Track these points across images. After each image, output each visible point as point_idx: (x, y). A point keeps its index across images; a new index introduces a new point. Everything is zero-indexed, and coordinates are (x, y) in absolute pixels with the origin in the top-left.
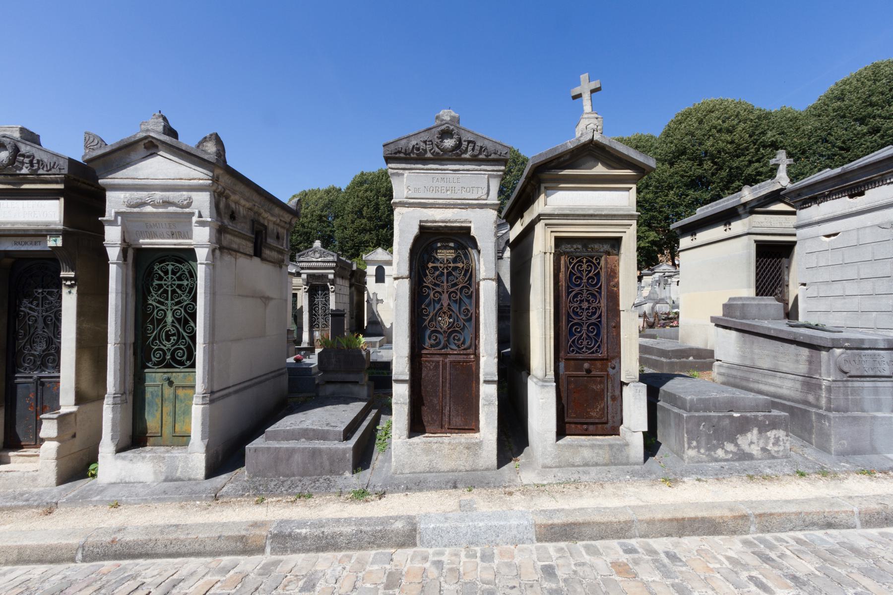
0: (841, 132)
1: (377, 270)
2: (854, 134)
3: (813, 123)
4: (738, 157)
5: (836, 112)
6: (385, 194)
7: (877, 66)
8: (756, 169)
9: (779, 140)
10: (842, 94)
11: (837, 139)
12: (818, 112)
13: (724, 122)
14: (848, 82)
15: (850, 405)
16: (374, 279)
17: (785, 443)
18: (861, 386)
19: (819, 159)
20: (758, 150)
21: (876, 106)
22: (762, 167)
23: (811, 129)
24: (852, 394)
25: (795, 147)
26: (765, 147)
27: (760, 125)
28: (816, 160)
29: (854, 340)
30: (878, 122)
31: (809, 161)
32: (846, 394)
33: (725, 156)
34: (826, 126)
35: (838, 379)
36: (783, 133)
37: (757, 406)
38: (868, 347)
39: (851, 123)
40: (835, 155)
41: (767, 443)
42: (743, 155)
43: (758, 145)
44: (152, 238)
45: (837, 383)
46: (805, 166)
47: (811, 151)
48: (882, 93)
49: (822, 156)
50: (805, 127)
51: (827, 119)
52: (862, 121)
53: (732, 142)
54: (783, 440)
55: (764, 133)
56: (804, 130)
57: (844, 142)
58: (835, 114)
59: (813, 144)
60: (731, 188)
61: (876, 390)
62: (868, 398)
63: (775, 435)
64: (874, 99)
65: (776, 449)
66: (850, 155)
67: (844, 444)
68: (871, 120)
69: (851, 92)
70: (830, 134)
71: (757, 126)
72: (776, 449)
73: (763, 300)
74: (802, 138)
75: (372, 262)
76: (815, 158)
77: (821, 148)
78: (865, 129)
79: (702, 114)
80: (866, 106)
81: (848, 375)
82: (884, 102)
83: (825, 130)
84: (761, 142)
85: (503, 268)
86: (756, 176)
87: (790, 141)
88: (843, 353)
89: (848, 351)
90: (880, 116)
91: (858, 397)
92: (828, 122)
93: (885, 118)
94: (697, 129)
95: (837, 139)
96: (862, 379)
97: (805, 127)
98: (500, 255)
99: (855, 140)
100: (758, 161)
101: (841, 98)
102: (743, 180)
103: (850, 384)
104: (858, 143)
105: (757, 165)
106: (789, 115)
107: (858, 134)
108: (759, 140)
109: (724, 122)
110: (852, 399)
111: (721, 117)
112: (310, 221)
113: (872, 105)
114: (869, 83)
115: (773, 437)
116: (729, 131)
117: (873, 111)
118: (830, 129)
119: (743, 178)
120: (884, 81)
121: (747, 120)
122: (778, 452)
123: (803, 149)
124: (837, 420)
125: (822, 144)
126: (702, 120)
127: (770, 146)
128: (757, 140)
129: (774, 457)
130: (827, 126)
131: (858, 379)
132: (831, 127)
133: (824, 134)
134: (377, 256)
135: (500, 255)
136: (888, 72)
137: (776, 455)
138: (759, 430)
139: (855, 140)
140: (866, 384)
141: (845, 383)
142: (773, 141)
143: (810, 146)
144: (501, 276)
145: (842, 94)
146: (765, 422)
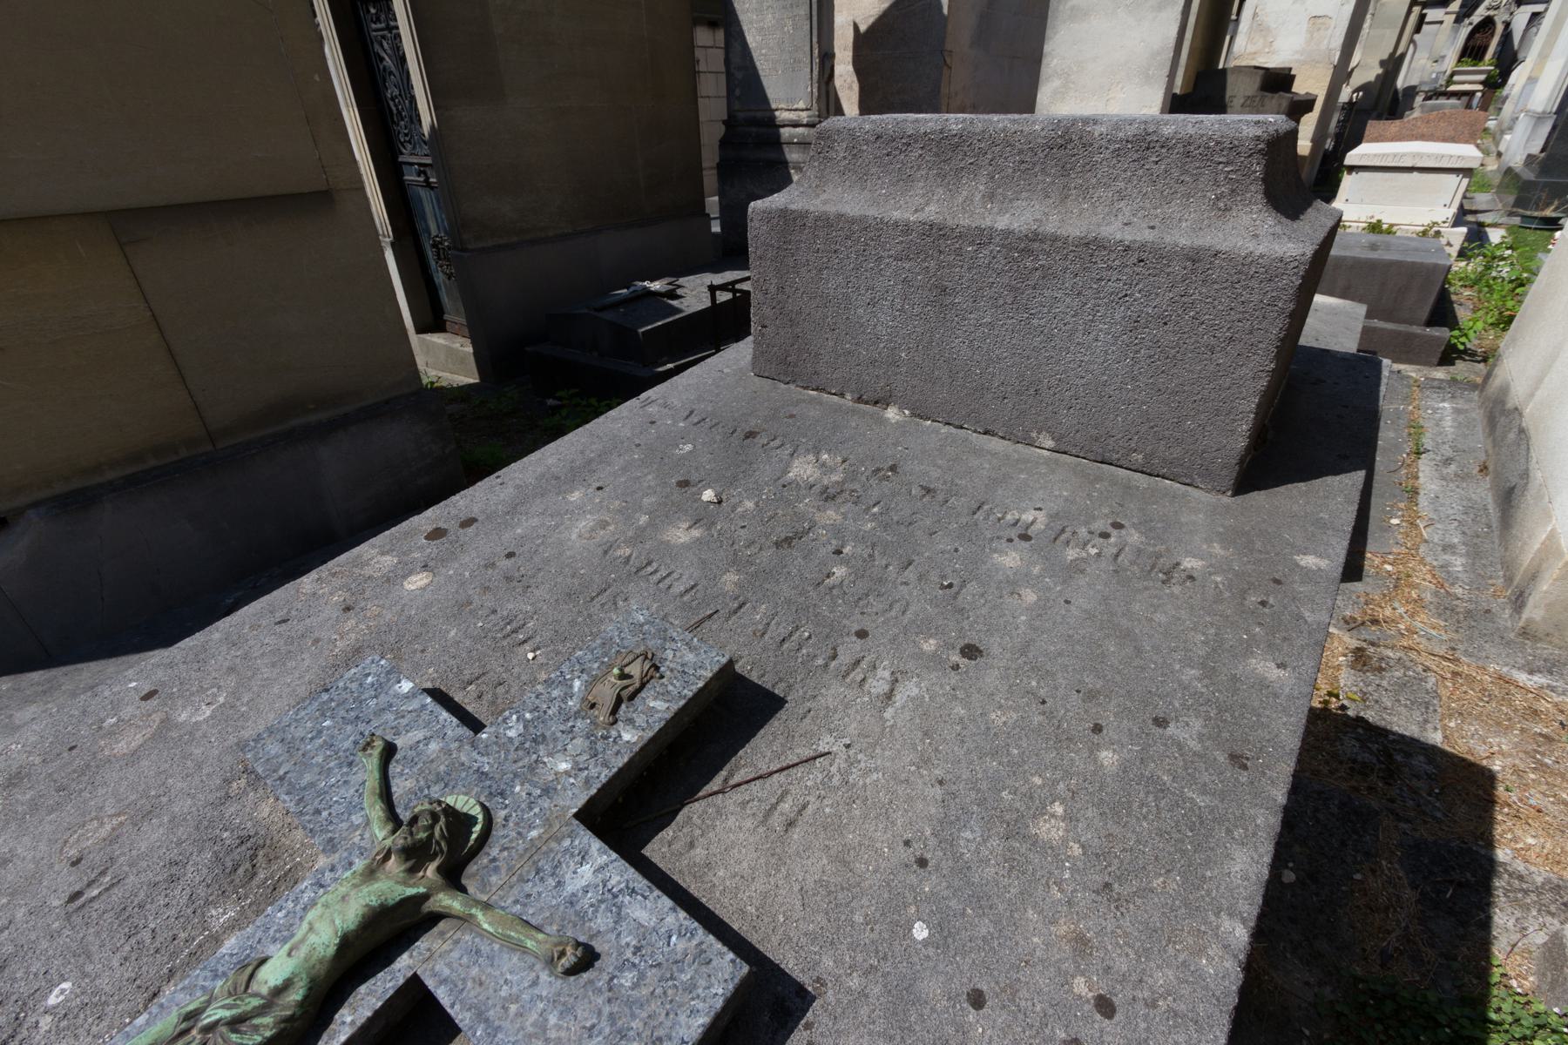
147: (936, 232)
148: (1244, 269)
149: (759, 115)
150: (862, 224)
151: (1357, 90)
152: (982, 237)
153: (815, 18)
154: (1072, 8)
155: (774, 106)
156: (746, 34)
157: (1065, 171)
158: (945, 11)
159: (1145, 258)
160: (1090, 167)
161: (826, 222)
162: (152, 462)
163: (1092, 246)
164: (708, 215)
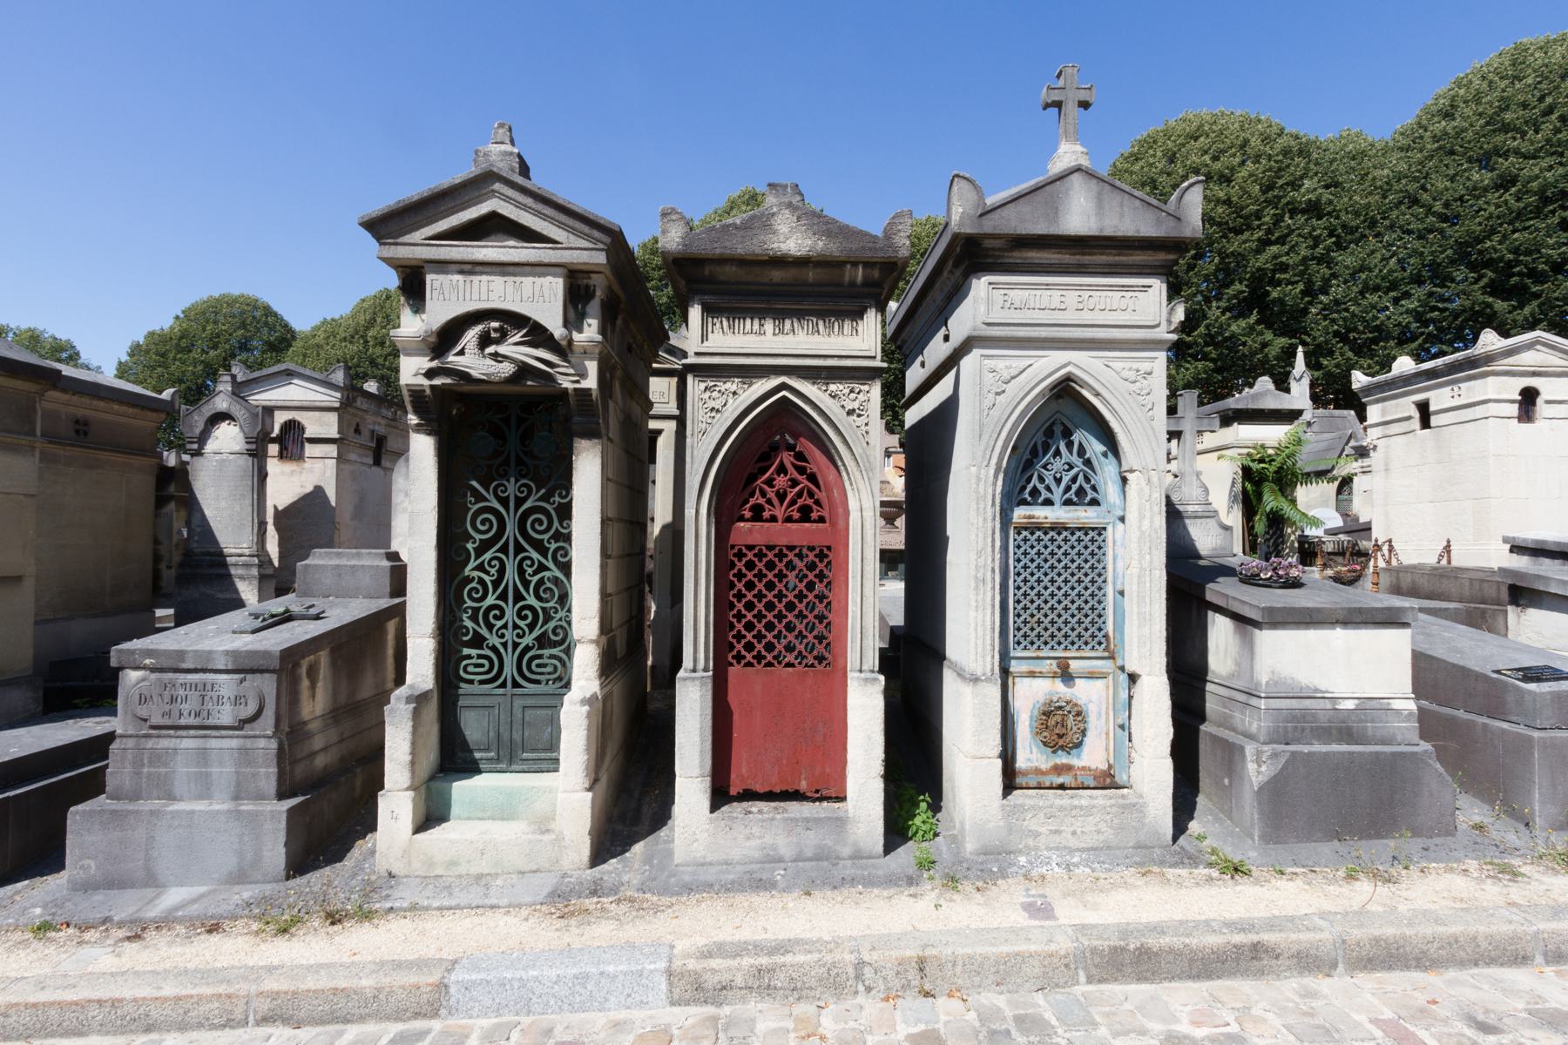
0: (1441, 184)
2: (1467, 188)
3: (1400, 164)
4: (1238, 232)
5: (1438, 142)
6: (1419, 275)
7: (1522, 50)
8: (1275, 257)
9: (1324, 200)
10: (1452, 106)
11: (1434, 199)
12: (1410, 141)
13: (1215, 158)
14: (1465, 81)
18: (172, 746)
19: (1401, 239)
20: (1278, 220)
21: (1512, 130)
22: (1287, 254)
23: (1388, 175)
24: (151, 764)
25: (1356, 212)
26: (1293, 213)
27: (1288, 166)
28: (1394, 239)
29: (166, 653)
30: (1513, 164)
31: (1381, 242)
32: (138, 763)
33: (1211, 231)
34: (1417, 171)
35: (130, 732)
36: (1336, 185)
39: (1462, 165)
40: (1430, 231)
42: (1249, 227)
43: (1283, 209)
44: (544, 371)
46: (1373, 252)
47: (1387, 222)
48: (1525, 106)
49: (1409, 232)
50: (1378, 173)
51: (1419, 155)
52: (1485, 161)
53: (1228, 202)
55: (1295, 185)
56: (1374, 179)
57: (1447, 205)
58: (1436, 145)
59: (1391, 208)
60: (1226, 297)
61: (203, 756)
62: (182, 770)
64: (1508, 116)
66: (1457, 231)
67: (89, 866)
68: (1500, 160)
69: (1469, 101)
70: (1423, 188)
71: (1280, 169)
74: (1371, 193)
76: (1394, 236)
77: (1405, 216)
78: (1486, 177)
79: (1175, 141)
80: (1494, 131)
82: (1526, 123)
83: (1416, 179)
84: (1288, 203)
85: (202, 474)
86: (1274, 271)
87: (1346, 199)
88: (144, 680)
89: (154, 676)
90: (1517, 152)
91: (163, 770)
92: (1421, 163)
93: (1526, 157)
94: (1162, 172)
95: (1434, 199)
97: (1378, 173)
99: (1469, 200)
100: (1281, 241)
101: (1448, 115)
102: (1248, 280)
103: (150, 743)
104: (1472, 206)
105: (1274, 249)
106: (1351, 146)
107: (1475, 189)
108: (1281, 197)
109: (1215, 158)
110: (150, 774)
111: (1210, 149)
112: (390, 354)
113: (1506, 128)
114: (1503, 84)
116: (1226, 179)
117: (1505, 142)
118: (1425, 178)
119: (1248, 276)
120: (1530, 81)
121: (1260, 156)
123: (1372, 218)
125: (1409, 208)
126: (1174, 154)
127: (1303, 212)
128: (1279, 198)
130: (1420, 171)
131: (172, 732)
132: (1427, 174)
133: (1414, 186)
136: (1540, 62)
139: (1469, 200)
141: (143, 740)
142: (1310, 200)
143: (1384, 212)
145: (1452, 106)
147: (338, 566)
148: (384, 568)
149: (212, 550)
150: (324, 566)
152: (346, 566)
155: (222, 546)
158: (333, 504)
159: (371, 567)
161: (316, 566)
163: (363, 566)
164: (650, 405)
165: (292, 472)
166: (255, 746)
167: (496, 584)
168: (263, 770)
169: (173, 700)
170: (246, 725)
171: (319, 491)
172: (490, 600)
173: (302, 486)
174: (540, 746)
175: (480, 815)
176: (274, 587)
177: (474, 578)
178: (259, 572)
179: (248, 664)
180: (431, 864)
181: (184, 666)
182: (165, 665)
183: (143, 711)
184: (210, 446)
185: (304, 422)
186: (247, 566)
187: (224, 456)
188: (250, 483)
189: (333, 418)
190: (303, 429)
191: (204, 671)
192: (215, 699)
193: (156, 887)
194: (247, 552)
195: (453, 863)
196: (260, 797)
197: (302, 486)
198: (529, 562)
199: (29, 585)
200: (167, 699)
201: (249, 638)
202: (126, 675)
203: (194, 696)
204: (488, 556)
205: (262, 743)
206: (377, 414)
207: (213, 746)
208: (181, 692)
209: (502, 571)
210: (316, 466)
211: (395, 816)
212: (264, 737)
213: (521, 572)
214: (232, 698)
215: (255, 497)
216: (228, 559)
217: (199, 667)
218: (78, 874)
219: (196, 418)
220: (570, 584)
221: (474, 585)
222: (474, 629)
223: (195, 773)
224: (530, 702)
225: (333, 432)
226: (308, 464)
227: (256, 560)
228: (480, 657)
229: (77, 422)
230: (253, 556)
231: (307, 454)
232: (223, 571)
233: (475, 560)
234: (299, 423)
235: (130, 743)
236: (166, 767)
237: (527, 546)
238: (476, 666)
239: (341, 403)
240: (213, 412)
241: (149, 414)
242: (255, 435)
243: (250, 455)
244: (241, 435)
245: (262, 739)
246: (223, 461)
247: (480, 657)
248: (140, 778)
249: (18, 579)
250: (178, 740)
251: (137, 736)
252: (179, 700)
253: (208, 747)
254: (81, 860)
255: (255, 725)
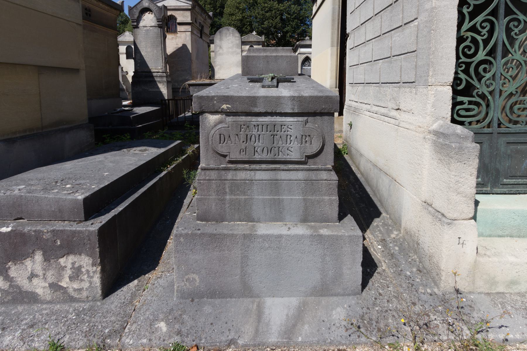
1: (127, 49)
15: (228, 210)
16: (125, 56)
17: (92, 277)
24: (232, 192)
32: (221, 192)
35: (212, 166)
37: (60, 211)
38: (262, 110)
41: (60, 277)
45: (208, 172)
54: (88, 271)
63: (73, 264)
65: (76, 285)
67: (194, 279)
72: (76, 285)
73: (277, 51)
75: (123, 43)
81: (228, 159)
88: (220, 122)
89: (230, 119)
96: (254, 166)
98: (135, 24)
103: (230, 175)
110: (231, 200)
115: (69, 266)
122: (80, 290)
124: (182, 239)
129: (72, 299)
131: (247, 166)
134: (126, 38)
135: (135, 24)
137: (76, 295)
138: (43, 255)
140: (260, 175)
141: (223, 172)
144: (137, 44)
146: (55, 241)
147: (267, 56)
149: (146, 70)
150: (258, 56)
151: (177, 160)
153: (163, 50)
154: (219, 53)
155: (151, 68)
156: (142, 52)
157: (277, 51)
158: (191, 52)
159: (287, 56)
160: (279, 51)
162: (28, 133)
163: (282, 56)
165: (172, 38)
166: (319, 178)
167: (486, 42)
168: (326, 198)
169: (248, 138)
170: (310, 160)
171: (184, 46)
172: (481, 55)
173: (177, 44)
174: (519, 174)
175: (500, 233)
176: (171, 88)
177: (467, 37)
178: (166, 79)
179: (311, 108)
180: (493, 282)
181: (256, 110)
182: (240, 109)
183: (222, 149)
184: (142, 24)
185: (176, 16)
186: (161, 77)
187: (148, 28)
188: (160, 40)
189: (188, 14)
190: (176, 19)
191: (272, 114)
192: (284, 138)
193: (251, 297)
194: (161, 71)
195: (513, 283)
196: (325, 220)
197: (177, 44)
198: (516, 23)
199: (83, 74)
200: (242, 137)
201: (484, 51)
202: (206, 118)
203: (265, 134)
204: (480, 18)
205: (324, 175)
206: (201, 15)
207: (283, 178)
208: (255, 132)
209: (491, 32)
210: (182, 35)
211: (461, 242)
212: (325, 170)
213: (508, 30)
214: (299, 137)
215: (163, 46)
216: (153, 74)
217: (269, 111)
218: (185, 285)
219: (135, 11)
220: (137, 113)
221: (467, 43)
222: (466, 80)
223: (270, 200)
224: (512, 139)
225: (189, 20)
226: (179, 34)
227: (165, 74)
228: (470, 103)
229: (86, 9)
230: (163, 72)
231: (178, 30)
232: (151, 79)
233: (469, 22)
234: (174, 16)
235: (213, 175)
236: (244, 195)
237: (515, 10)
238: (467, 110)
239: (192, 7)
240: (142, 7)
241: (114, 10)
242: (161, 18)
243: (159, 27)
244: (155, 18)
245: (323, 172)
246: (148, 30)
247: (470, 103)
248: (224, 204)
249: (77, 71)
250: (252, 173)
251: (218, 169)
252: (253, 139)
253: (279, 178)
254: (186, 275)
255: (317, 159)
